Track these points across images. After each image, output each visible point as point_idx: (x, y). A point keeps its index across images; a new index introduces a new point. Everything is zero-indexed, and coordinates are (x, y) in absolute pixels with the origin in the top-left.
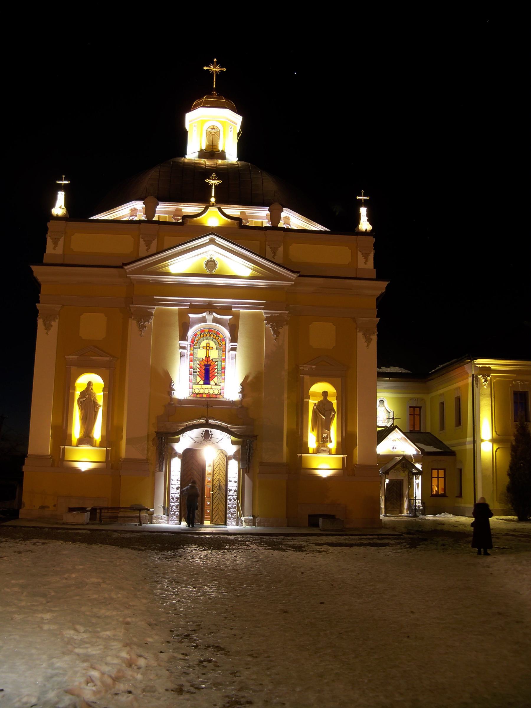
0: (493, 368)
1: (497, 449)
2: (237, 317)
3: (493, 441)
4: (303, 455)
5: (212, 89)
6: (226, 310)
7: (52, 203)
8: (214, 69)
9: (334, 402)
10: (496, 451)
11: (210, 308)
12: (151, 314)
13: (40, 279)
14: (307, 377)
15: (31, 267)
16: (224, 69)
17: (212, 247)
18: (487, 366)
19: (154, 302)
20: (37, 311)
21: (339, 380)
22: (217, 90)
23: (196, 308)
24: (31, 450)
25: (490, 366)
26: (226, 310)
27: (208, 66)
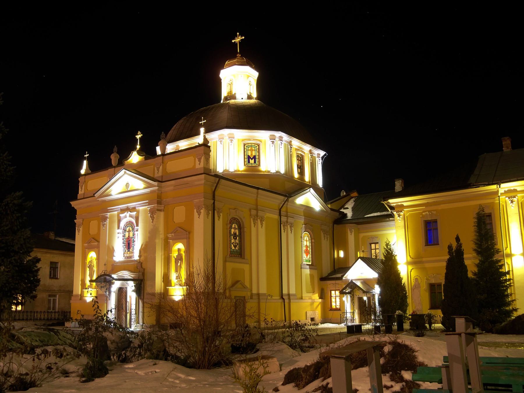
0: (405, 204)
1: (411, 270)
2: (138, 212)
3: (408, 263)
4: (169, 287)
5: (237, 53)
6: (134, 209)
7: (81, 167)
8: (238, 40)
9: (184, 254)
10: (411, 271)
11: (128, 209)
12: (107, 218)
13: (75, 208)
14: (171, 241)
15: (71, 203)
16: (243, 38)
17: (126, 175)
18: (400, 204)
19: (108, 211)
20: (75, 224)
21: (185, 240)
22: (240, 53)
23: (123, 211)
24: (74, 293)
25: (402, 203)
26: (134, 209)
27: (234, 39)
